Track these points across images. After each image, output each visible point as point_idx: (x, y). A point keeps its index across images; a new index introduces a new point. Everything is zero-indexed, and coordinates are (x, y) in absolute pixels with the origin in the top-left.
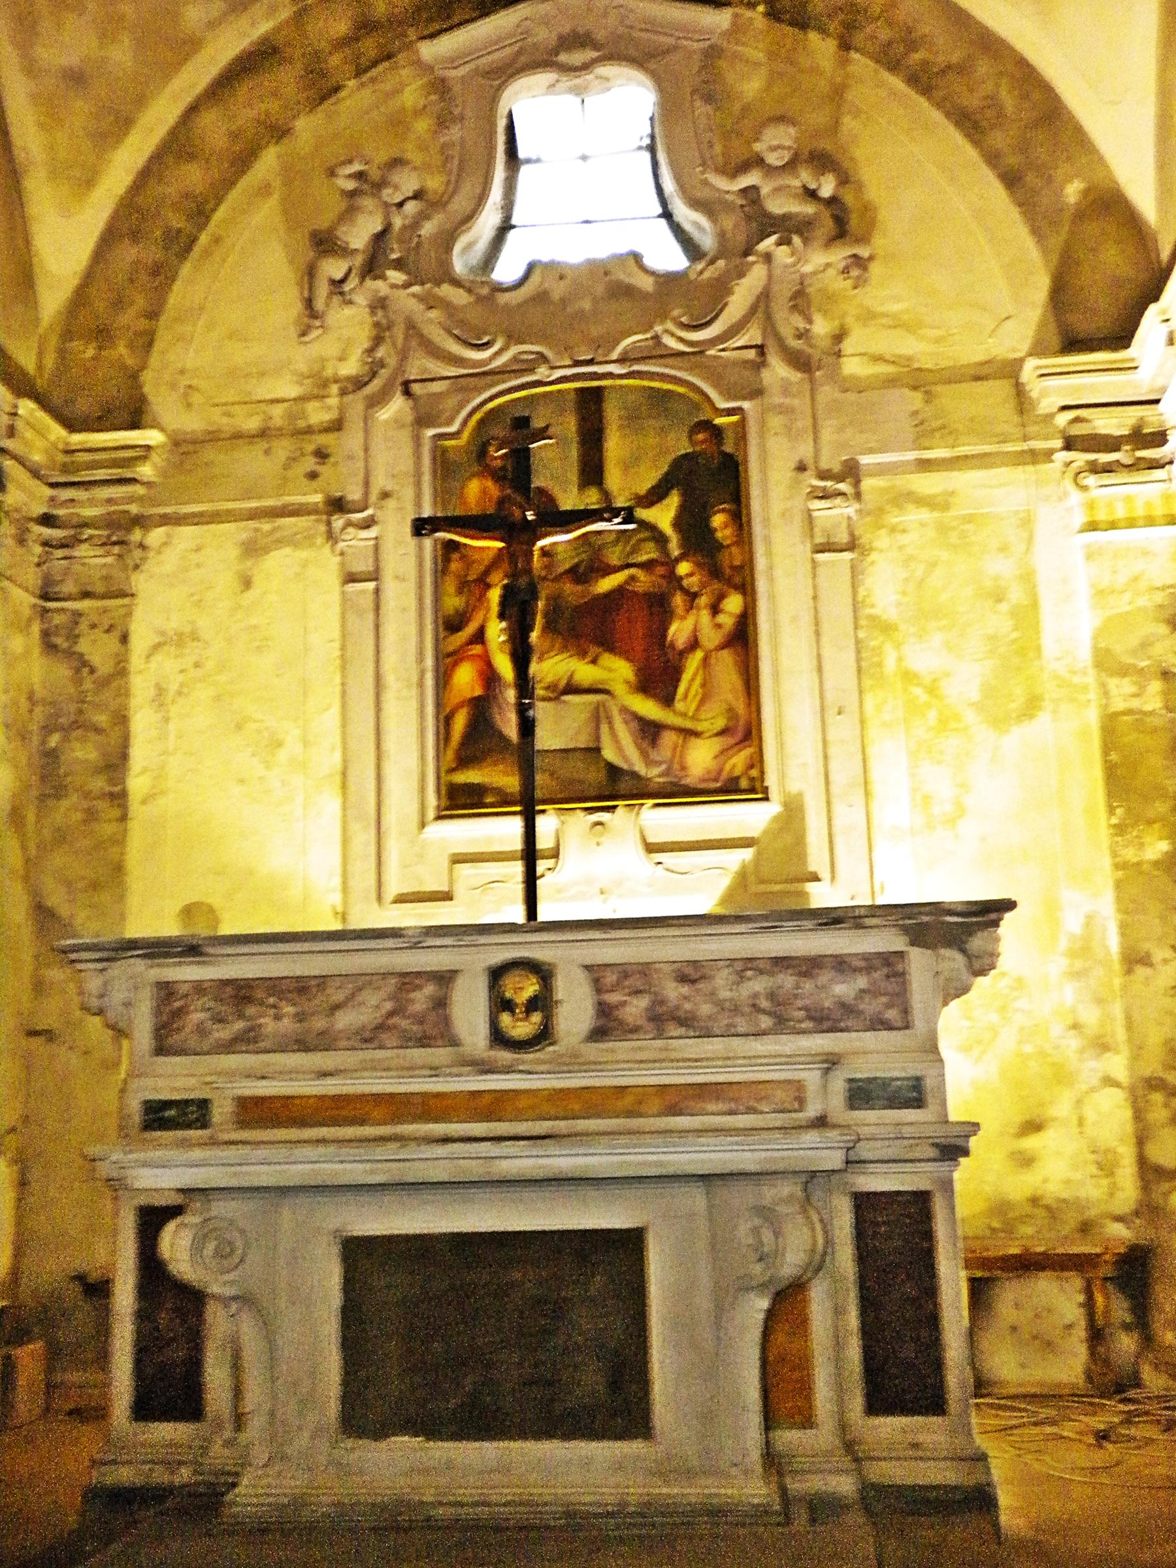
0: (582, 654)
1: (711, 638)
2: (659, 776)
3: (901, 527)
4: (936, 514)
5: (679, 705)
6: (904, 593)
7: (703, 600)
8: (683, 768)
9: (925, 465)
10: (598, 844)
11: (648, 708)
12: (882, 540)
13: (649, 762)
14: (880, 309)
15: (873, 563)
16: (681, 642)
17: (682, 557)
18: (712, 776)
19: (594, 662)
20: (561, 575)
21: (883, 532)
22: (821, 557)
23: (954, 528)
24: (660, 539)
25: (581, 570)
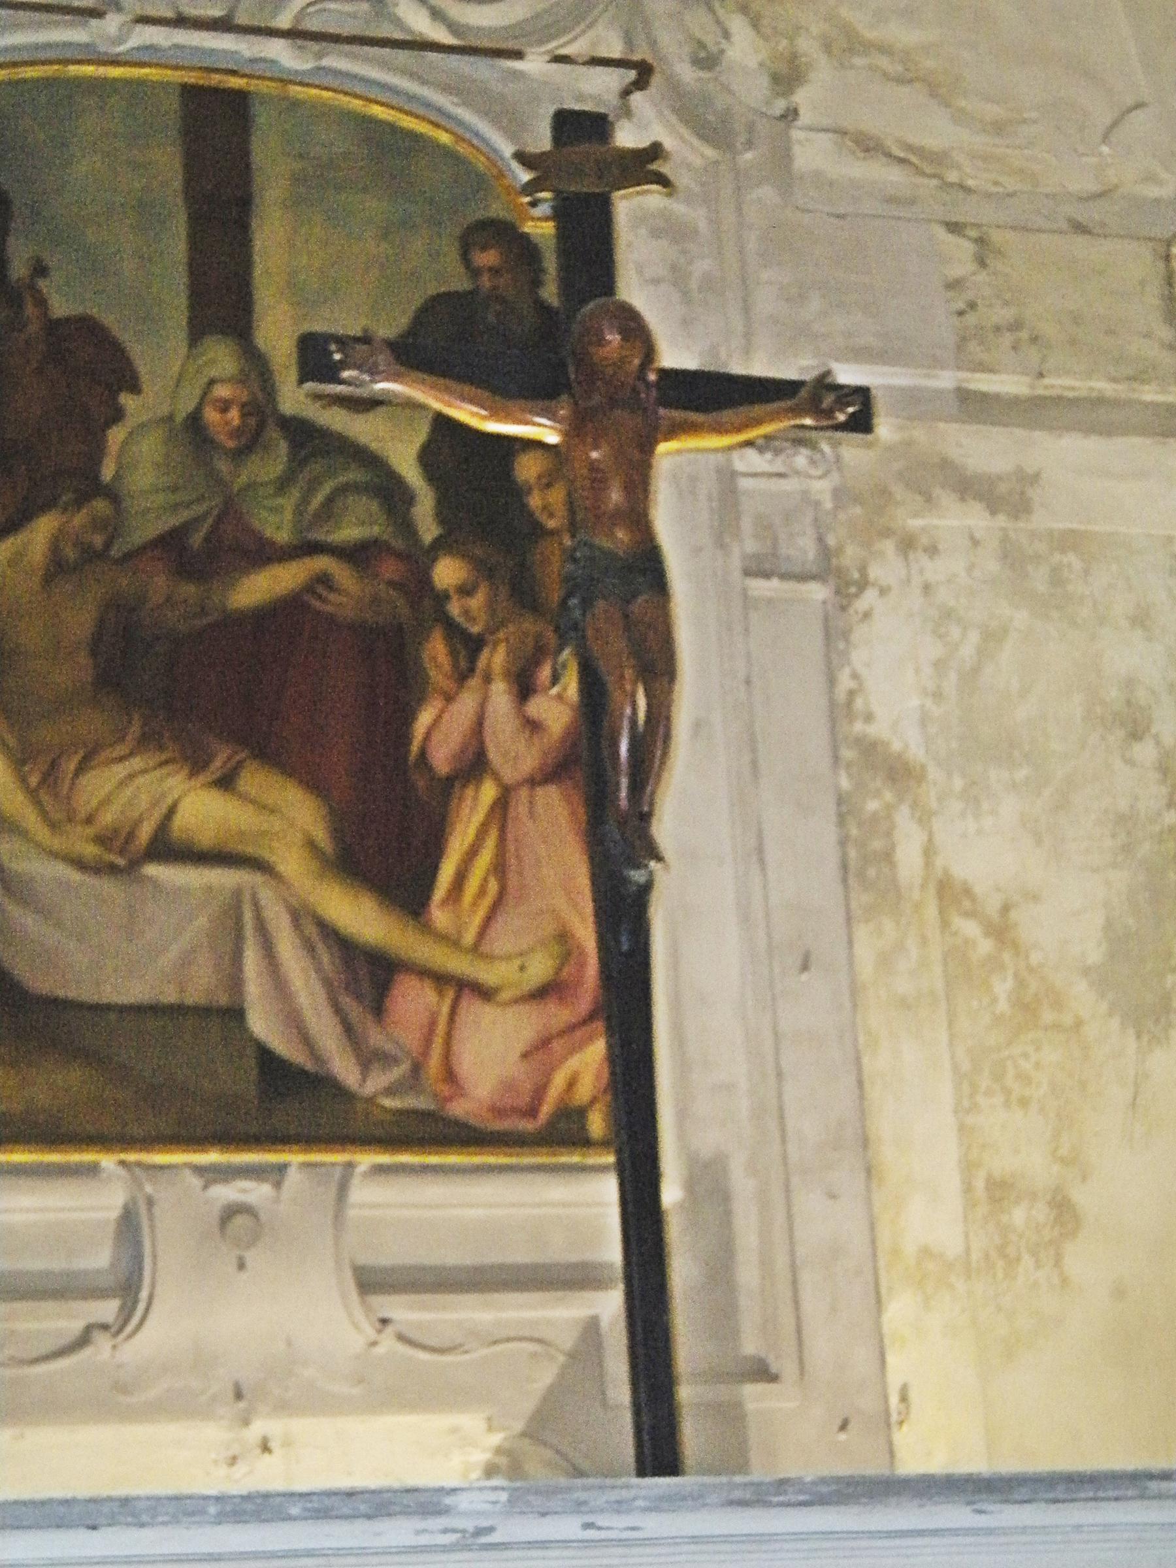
0: (196, 763)
1: (514, 754)
2: (390, 1091)
3: (924, 540)
4: (1002, 520)
5: (440, 916)
6: (938, 695)
7: (496, 658)
8: (450, 1075)
9: (975, 407)
10: (241, 1266)
11: (361, 917)
12: (886, 568)
13: (368, 1059)
14: (870, 35)
15: (867, 615)
16: (442, 759)
17: (440, 546)
18: (524, 1100)
19: (226, 783)
20: (144, 548)
21: (888, 546)
22: (761, 587)
23: (1037, 558)
24: (391, 493)
25: (196, 540)
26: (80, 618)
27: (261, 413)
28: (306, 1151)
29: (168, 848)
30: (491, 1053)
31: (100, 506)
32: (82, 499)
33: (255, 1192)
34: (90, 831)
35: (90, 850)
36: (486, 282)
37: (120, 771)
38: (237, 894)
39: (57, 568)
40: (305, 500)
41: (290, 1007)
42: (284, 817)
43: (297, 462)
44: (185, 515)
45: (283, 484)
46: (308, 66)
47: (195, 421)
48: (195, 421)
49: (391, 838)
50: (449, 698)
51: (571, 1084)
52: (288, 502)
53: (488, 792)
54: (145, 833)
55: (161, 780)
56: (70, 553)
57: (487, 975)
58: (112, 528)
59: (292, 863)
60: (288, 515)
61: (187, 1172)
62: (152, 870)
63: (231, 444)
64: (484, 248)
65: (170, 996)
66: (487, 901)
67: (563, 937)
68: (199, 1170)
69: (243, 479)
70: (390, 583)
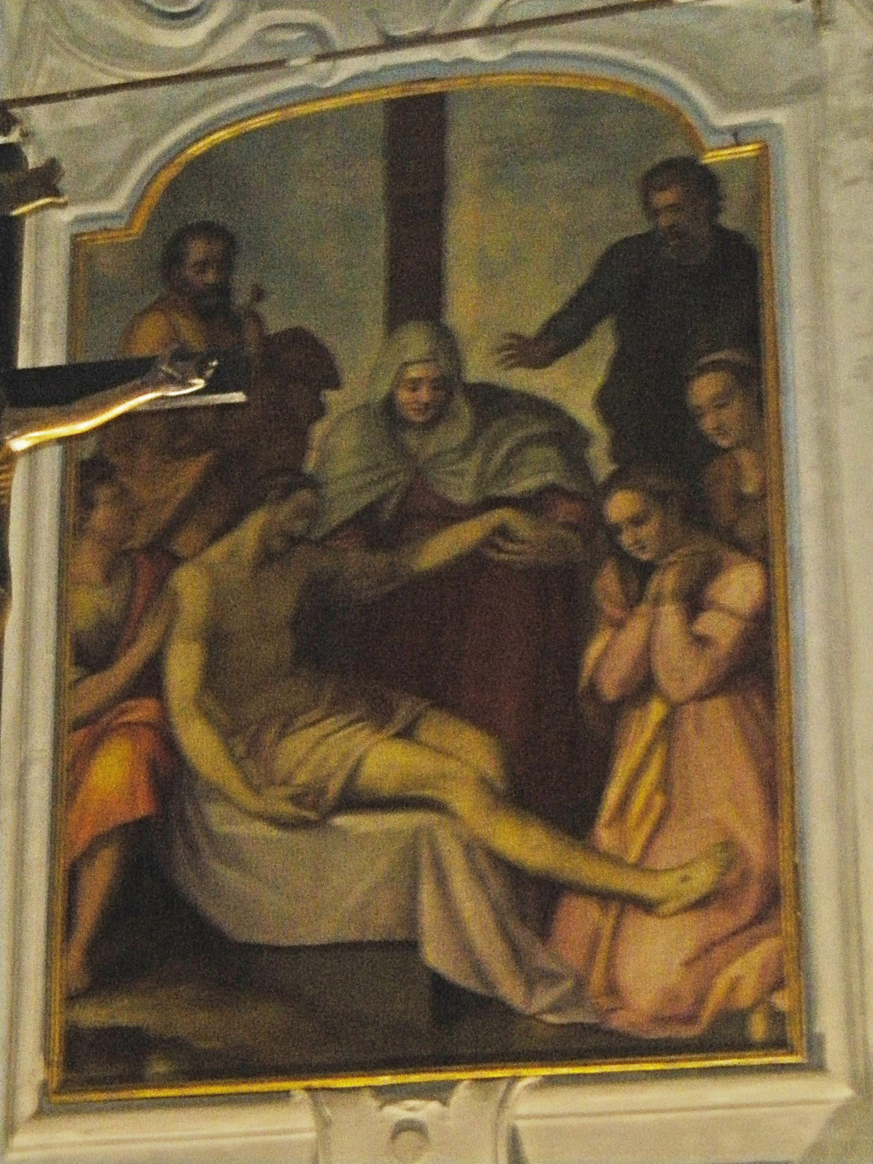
0: (379, 716)
1: (681, 669)
2: (554, 1009)
5: (605, 837)
7: (667, 581)
8: (612, 989)
11: (528, 845)
13: (533, 979)
17: (616, 481)
18: (685, 1006)
19: (407, 734)
20: (341, 527)
24: (567, 437)
26: (282, 601)
27: (448, 384)
28: (471, 1070)
29: (356, 799)
30: (652, 963)
31: (304, 496)
32: (288, 491)
33: (425, 1110)
34: (288, 791)
35: (287, 809)
36: (664, 221)
37: (314, 733)
38: (416, 834)
39: (266, 557)
40: (486, 460)
41: (461, 933)
42: (457, 759)
43: (481, 423)
44: (380, 489)
45: (466, 450)
46: (501, 55)
47: (389, 403)
48: (389, 403)
49: (559, 769)
50: (619, 625)
51: (734, 987)
52: (471, 465)
53: (656, 711)
54: (334, 787)
55: (348, 738)
56: (277, 544)
57: (648, 888)
58: (312, 514)
59: (464, 801)
60: (470, 479)
61: (367, 1093)
62: (341, 821)
63: (420, 419)
64: (662, 189)
65: (351, 935)
66: (653, 817)
67: (728, 844)
68: (378, 1091)
69: (431, 449)
70: (565, 525)
